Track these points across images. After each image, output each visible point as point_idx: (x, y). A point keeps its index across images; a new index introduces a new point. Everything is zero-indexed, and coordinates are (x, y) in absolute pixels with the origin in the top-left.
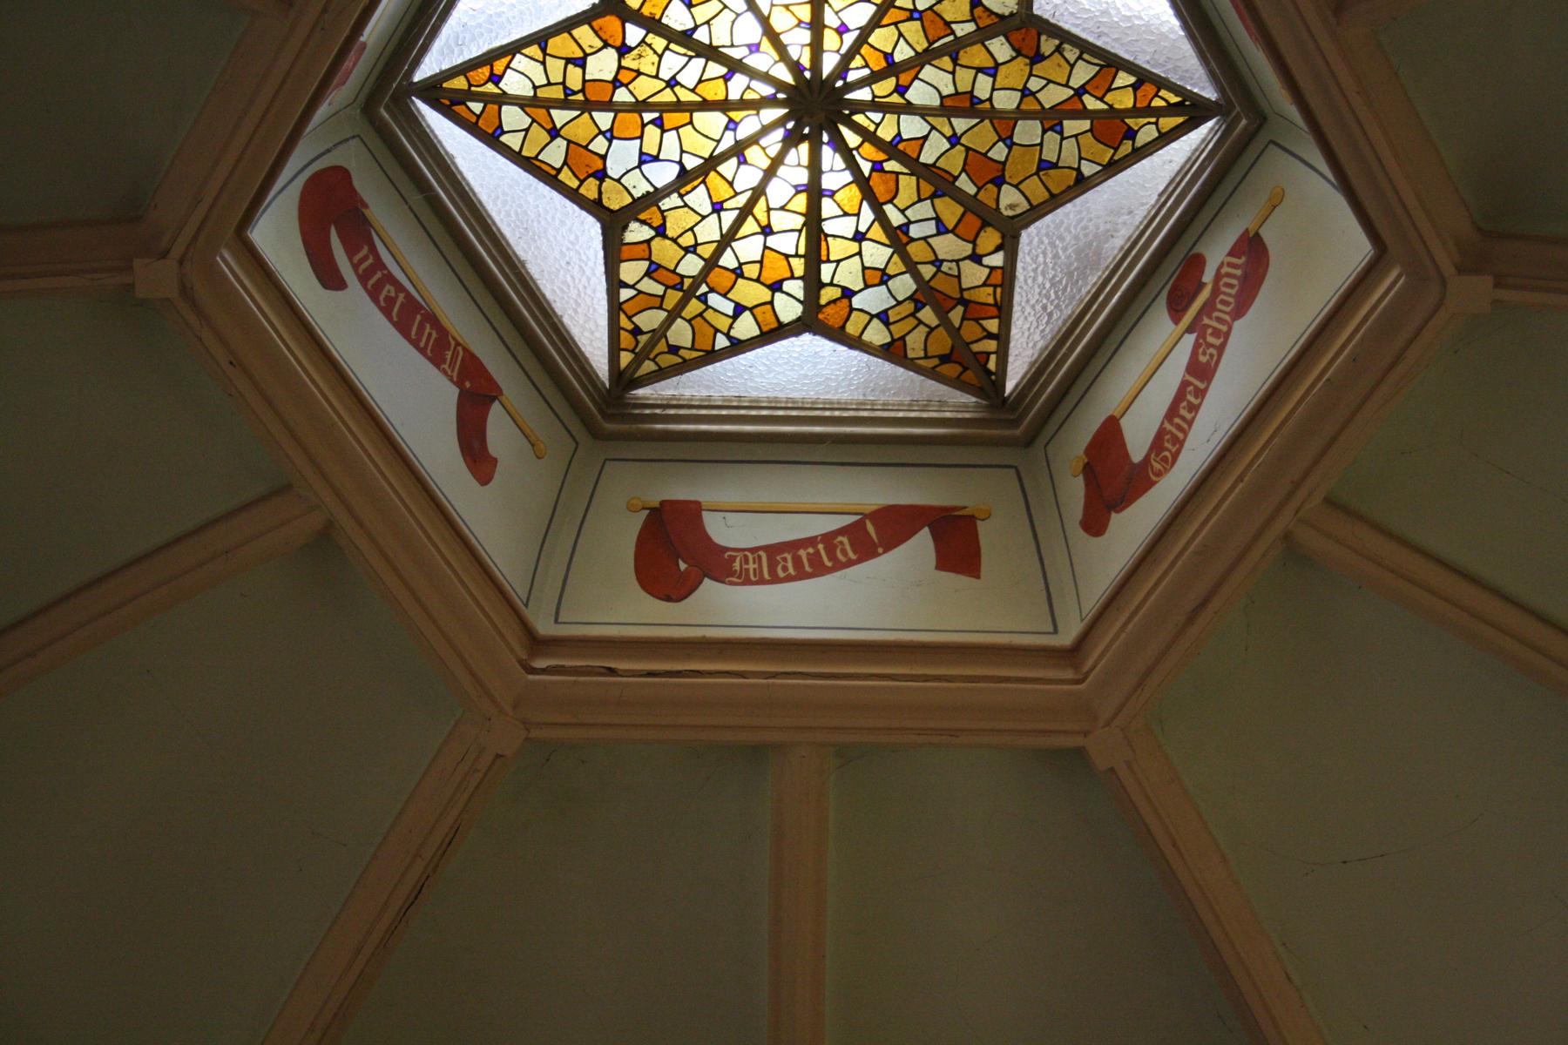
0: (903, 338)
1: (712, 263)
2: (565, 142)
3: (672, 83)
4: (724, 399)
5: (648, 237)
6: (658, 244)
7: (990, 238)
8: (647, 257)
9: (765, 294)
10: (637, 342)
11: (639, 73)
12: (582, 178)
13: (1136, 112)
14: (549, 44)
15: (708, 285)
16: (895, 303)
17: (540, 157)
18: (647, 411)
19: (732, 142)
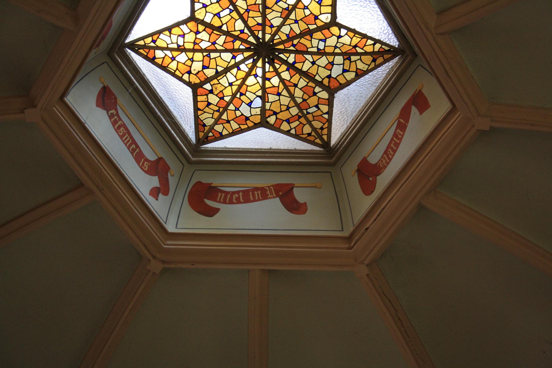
0: (357, 69)
1: (297, 105)
4: (350, 123)
5: (275, 118)
6: (278, 116)
10: (314, 136)
11: (222, 91)
16: (342, 65)
18: (338, 146)
19: (261, 79)
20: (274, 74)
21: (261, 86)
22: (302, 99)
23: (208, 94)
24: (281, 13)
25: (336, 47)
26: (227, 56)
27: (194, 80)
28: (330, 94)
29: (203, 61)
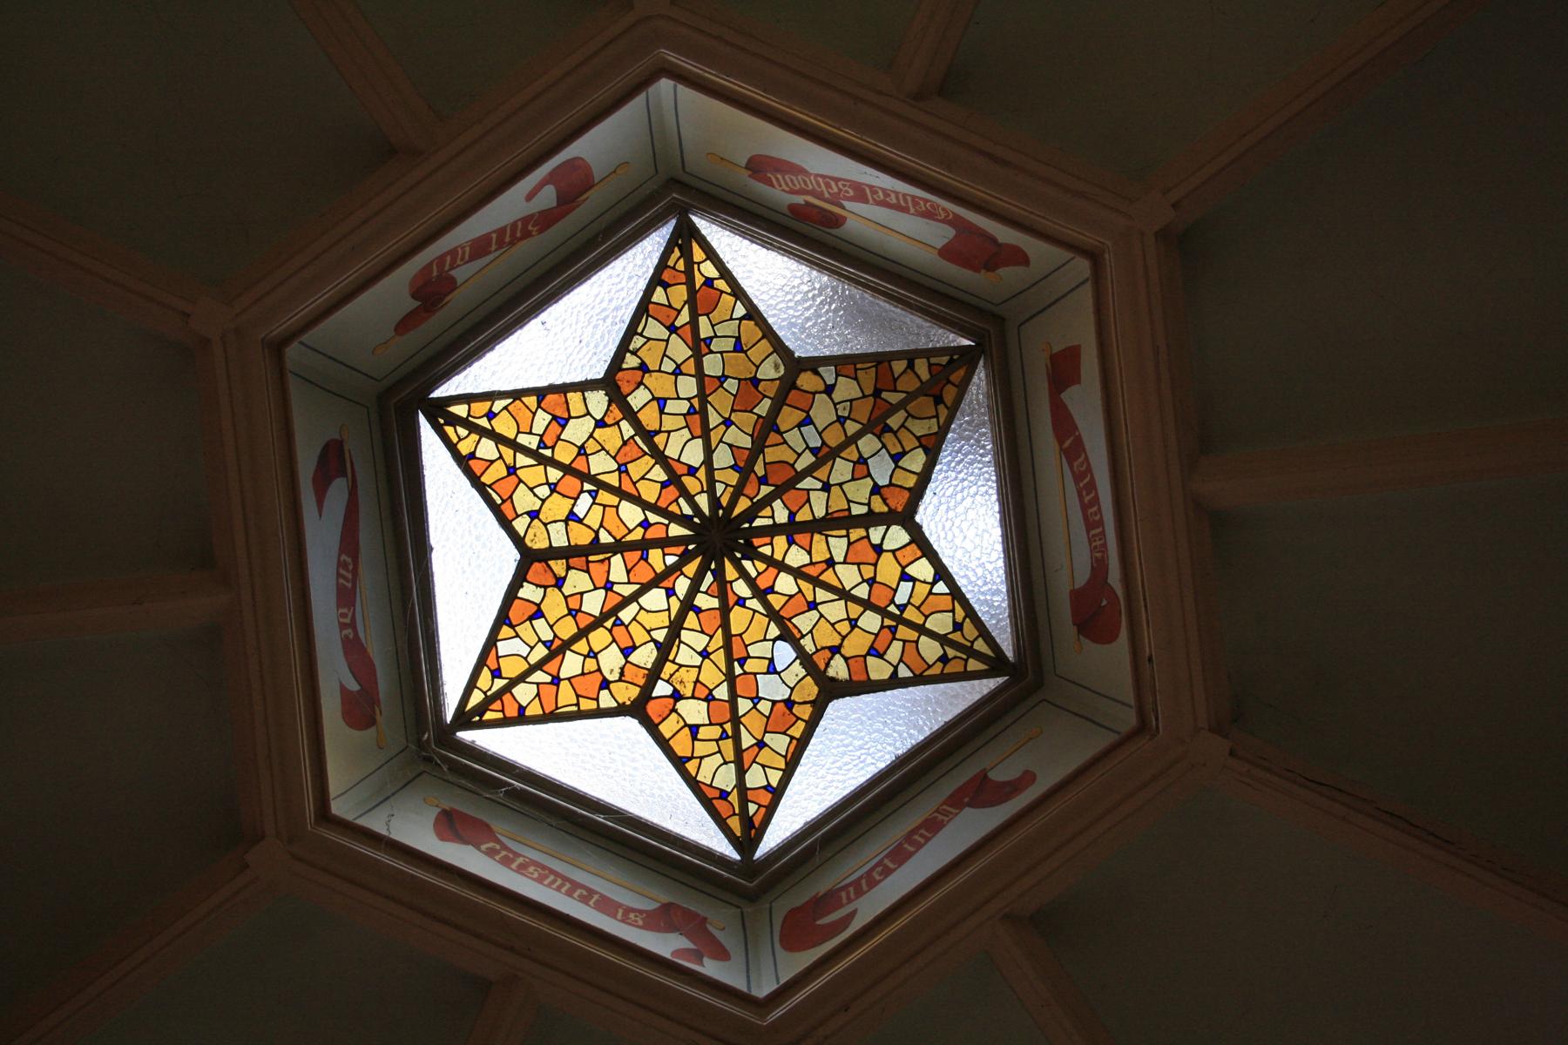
0: (918, 438)
1: (867, 605)
2: (767, 735)
3: (705, 654)
6: (848, 650)
7: (806, 381)
8: (862, 659)
9: (887, 558)
10: (955, 657)
11: (697, 681)
12: (795, 719)
13: (690, 282)
14: (682, 755)
15: (888, 606)
17: (784, 754)
20: (772, 571)
21: (765, 613)
22: (865, 584)
23: (675, 705)
24: (687, 426)
25: (842, 420)
26: (655, 598)
27: (628, 693)
28: (904, 520)
29: (614, 640)
